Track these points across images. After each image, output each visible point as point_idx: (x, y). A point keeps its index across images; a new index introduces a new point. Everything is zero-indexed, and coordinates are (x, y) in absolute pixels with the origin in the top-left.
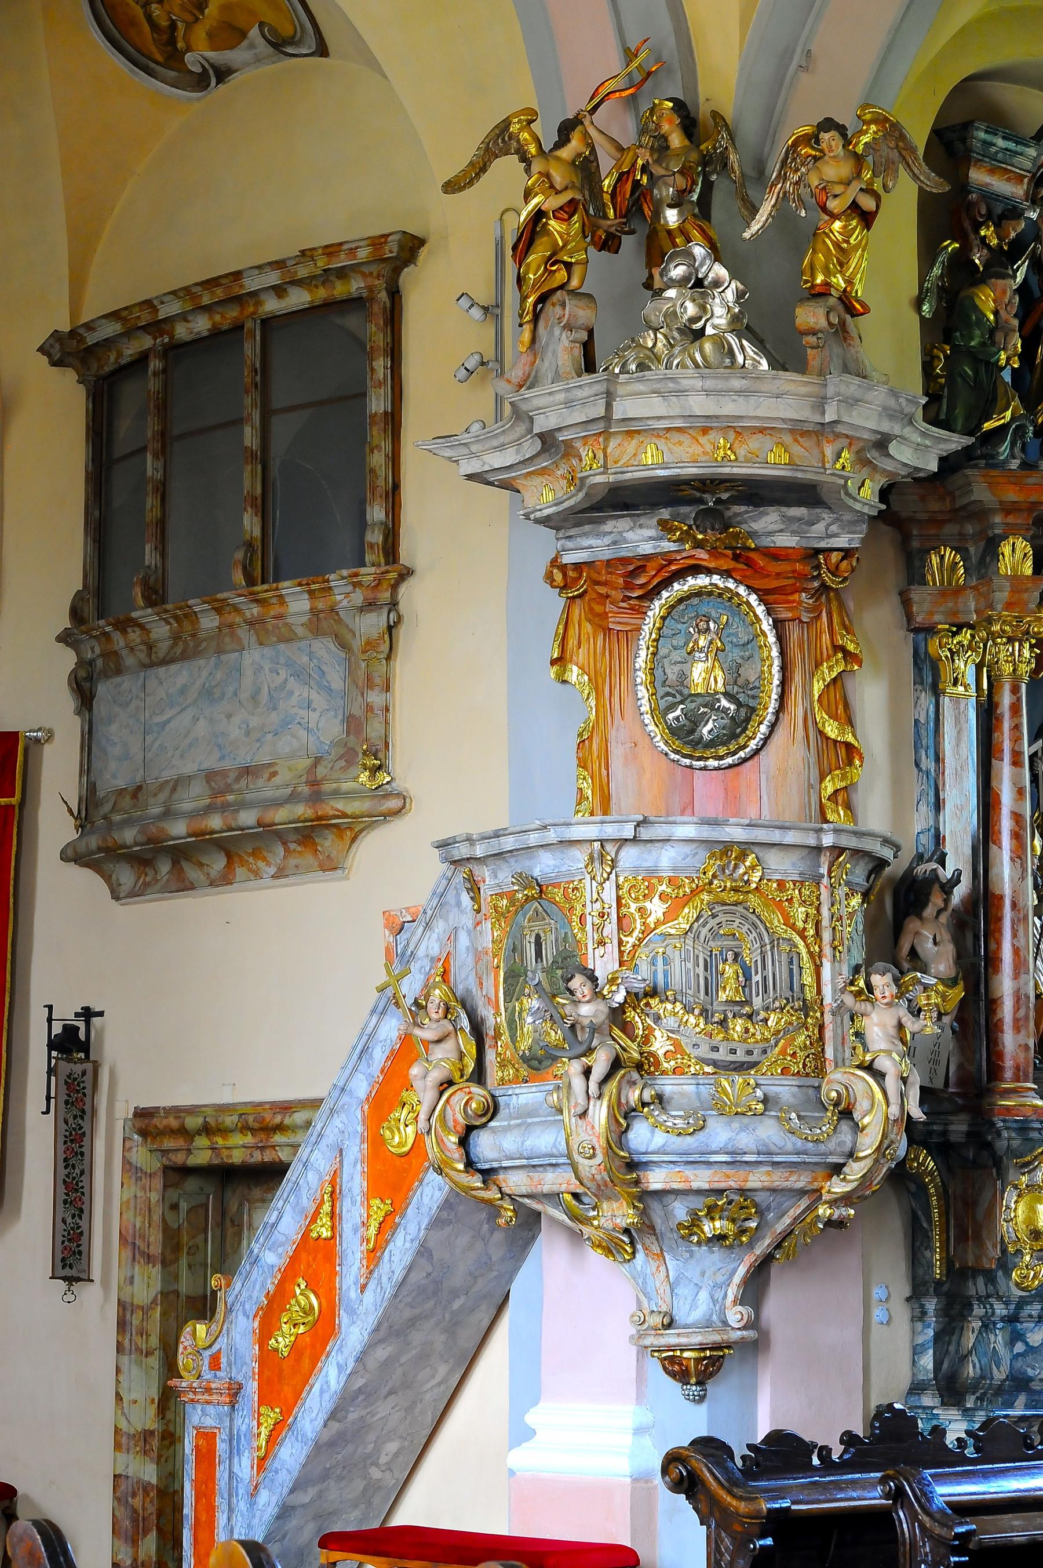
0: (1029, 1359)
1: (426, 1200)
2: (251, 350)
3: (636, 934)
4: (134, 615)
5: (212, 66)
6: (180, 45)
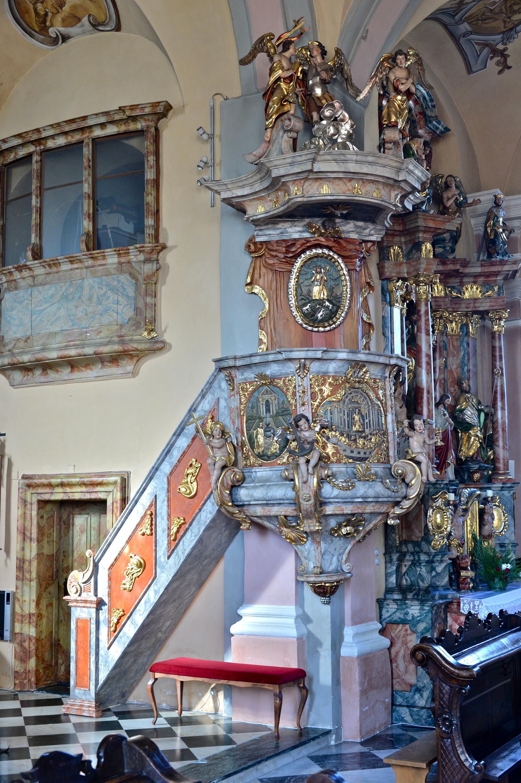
0: (437, 578)
1: (203, 518)
2: (87, 151)
3: (318, 400)
4: (28, 263)
5: (61, 34)
6: (48, 24)
